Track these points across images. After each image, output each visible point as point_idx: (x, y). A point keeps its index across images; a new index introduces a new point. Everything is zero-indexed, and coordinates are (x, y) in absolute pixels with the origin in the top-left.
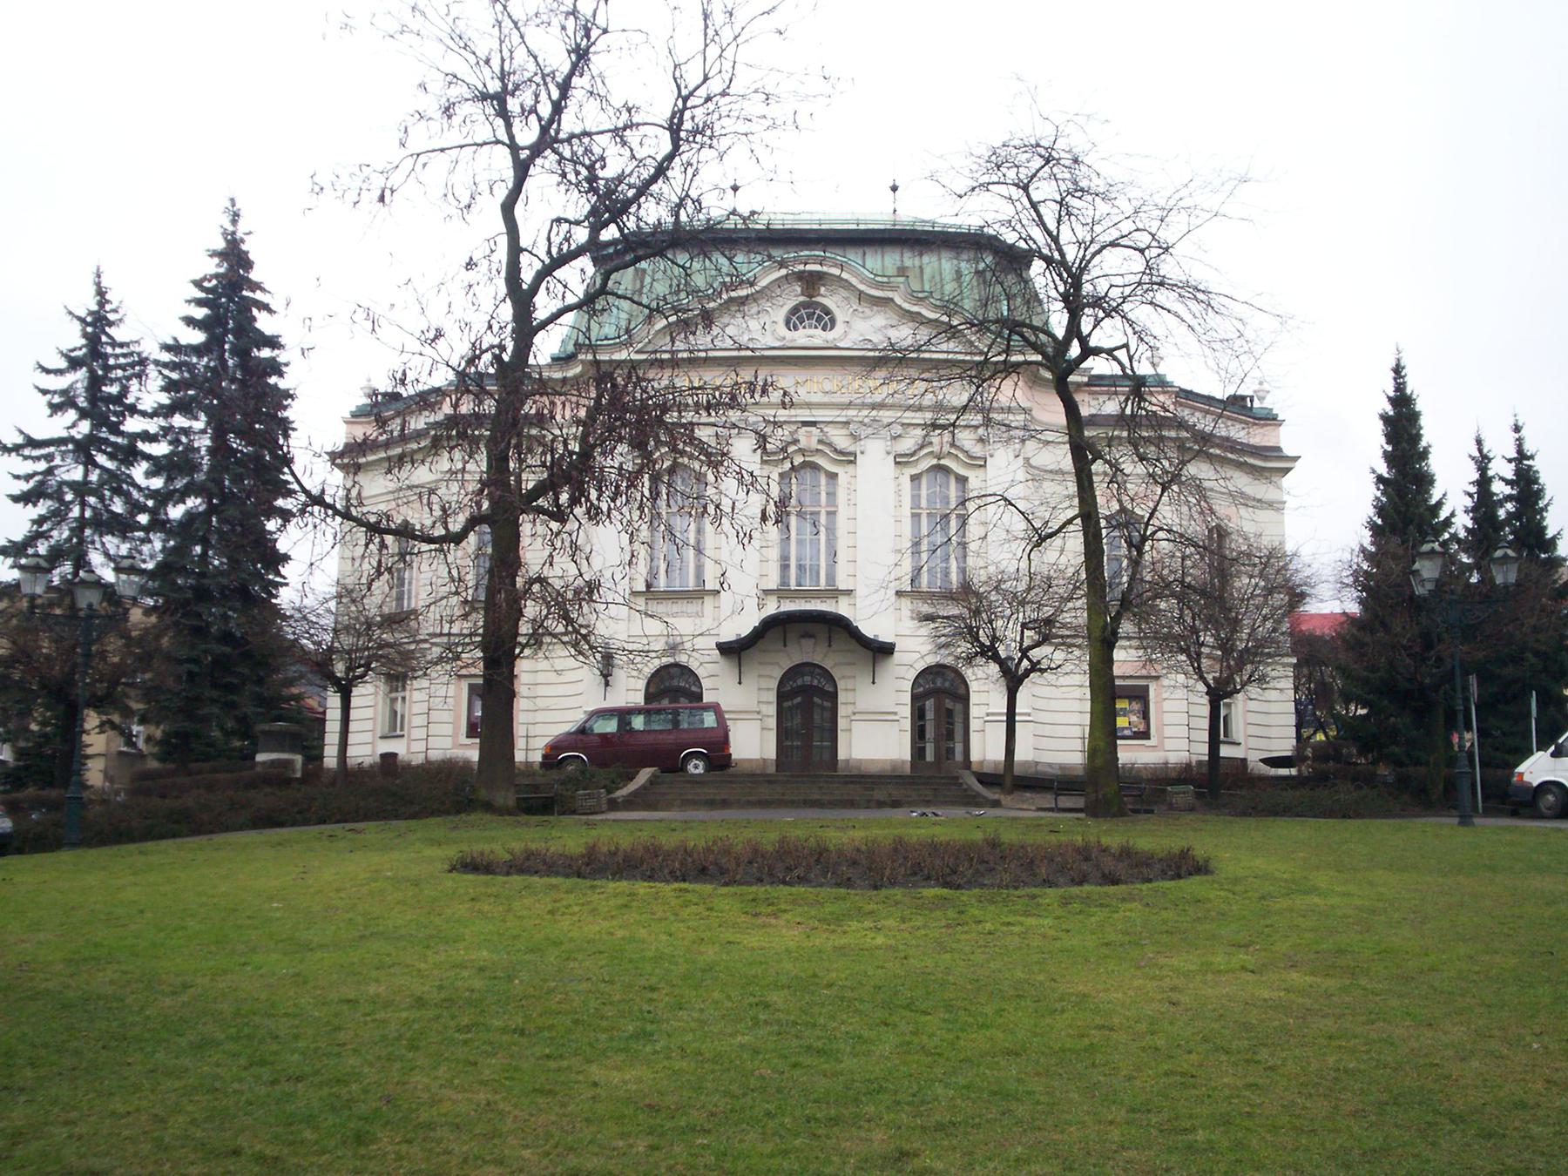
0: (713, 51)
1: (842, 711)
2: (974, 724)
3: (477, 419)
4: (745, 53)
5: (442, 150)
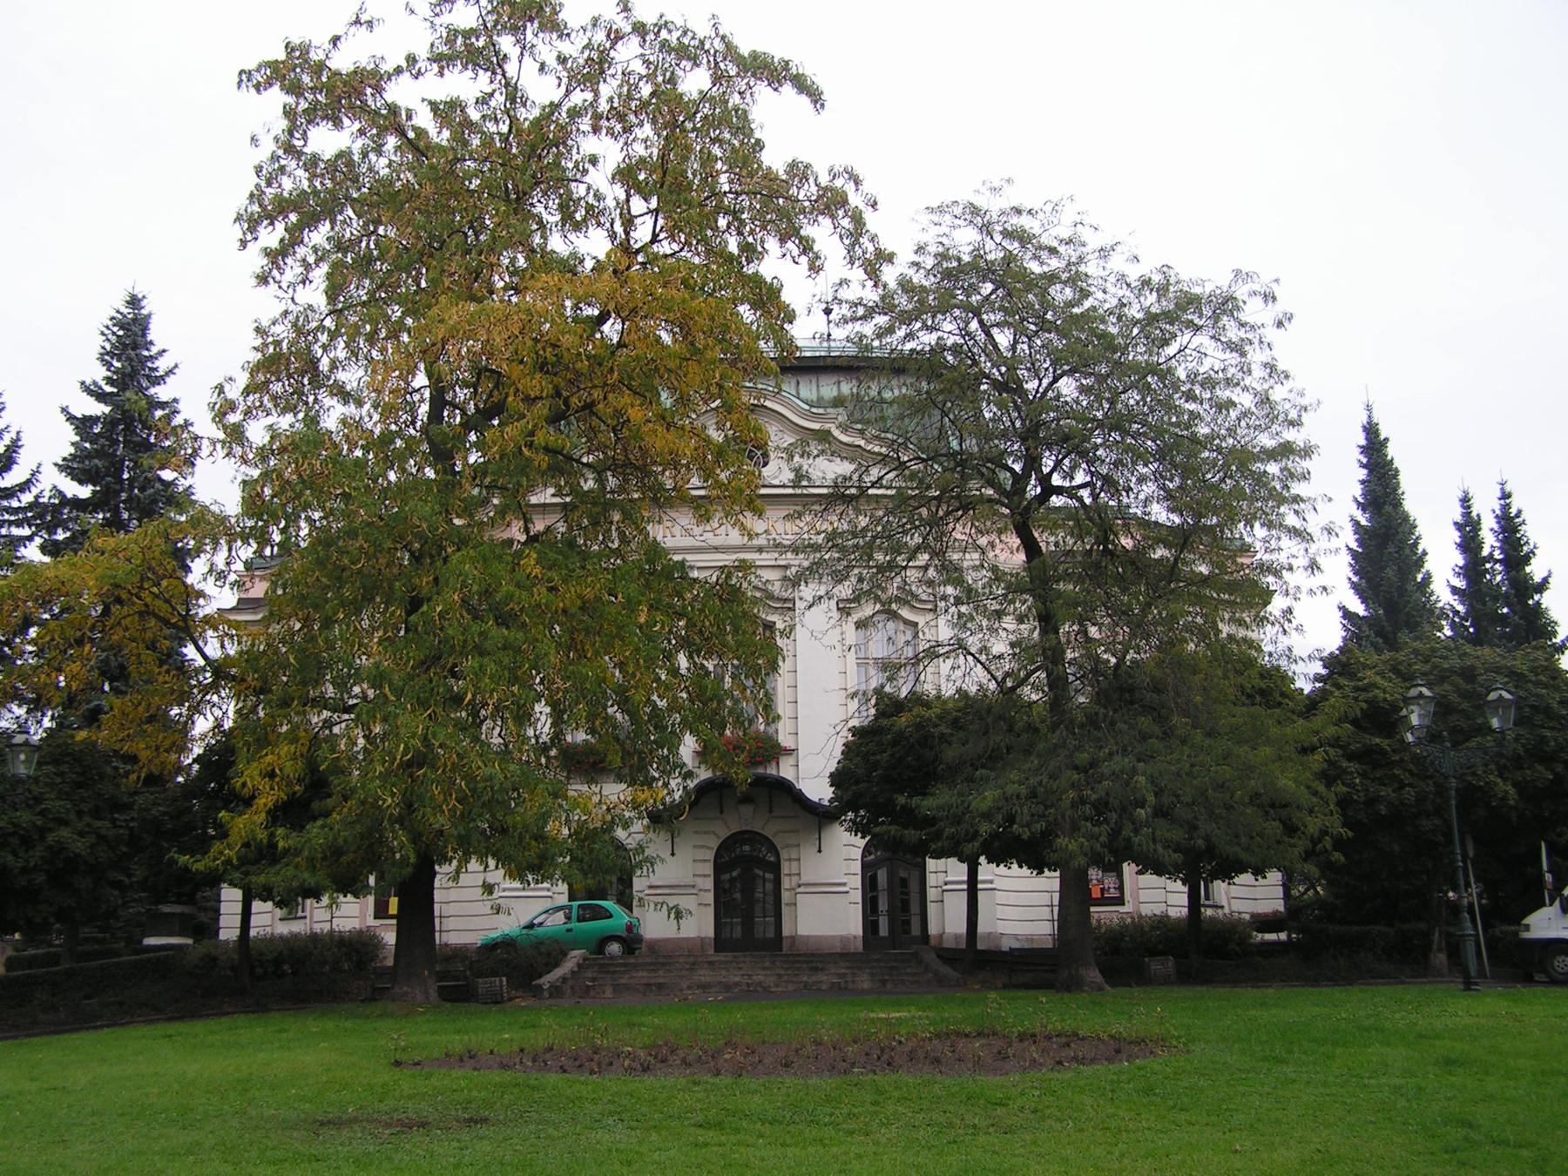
1: (786, 883)
2: (932, 894)
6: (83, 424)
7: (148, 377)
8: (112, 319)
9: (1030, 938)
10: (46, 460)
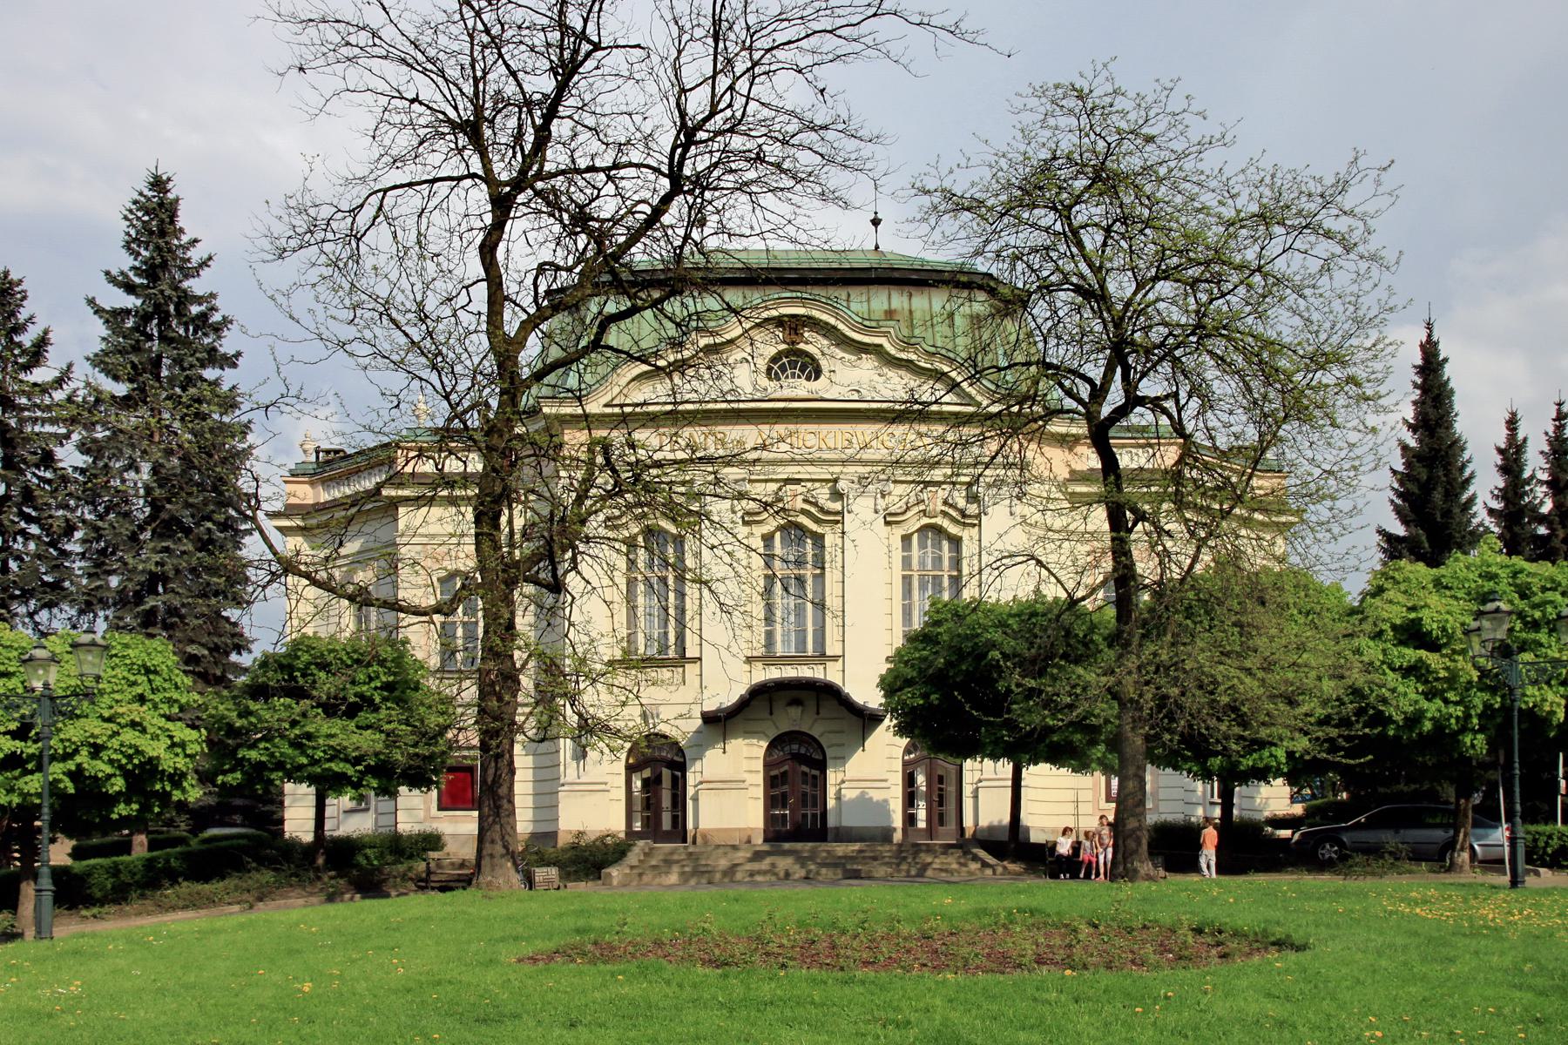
0: (723, 82)
3: (466, 479)
4: (761, 90)
5: (410, 185)
6: (114, 317)
7: (181, 268)
8: (135, 202)
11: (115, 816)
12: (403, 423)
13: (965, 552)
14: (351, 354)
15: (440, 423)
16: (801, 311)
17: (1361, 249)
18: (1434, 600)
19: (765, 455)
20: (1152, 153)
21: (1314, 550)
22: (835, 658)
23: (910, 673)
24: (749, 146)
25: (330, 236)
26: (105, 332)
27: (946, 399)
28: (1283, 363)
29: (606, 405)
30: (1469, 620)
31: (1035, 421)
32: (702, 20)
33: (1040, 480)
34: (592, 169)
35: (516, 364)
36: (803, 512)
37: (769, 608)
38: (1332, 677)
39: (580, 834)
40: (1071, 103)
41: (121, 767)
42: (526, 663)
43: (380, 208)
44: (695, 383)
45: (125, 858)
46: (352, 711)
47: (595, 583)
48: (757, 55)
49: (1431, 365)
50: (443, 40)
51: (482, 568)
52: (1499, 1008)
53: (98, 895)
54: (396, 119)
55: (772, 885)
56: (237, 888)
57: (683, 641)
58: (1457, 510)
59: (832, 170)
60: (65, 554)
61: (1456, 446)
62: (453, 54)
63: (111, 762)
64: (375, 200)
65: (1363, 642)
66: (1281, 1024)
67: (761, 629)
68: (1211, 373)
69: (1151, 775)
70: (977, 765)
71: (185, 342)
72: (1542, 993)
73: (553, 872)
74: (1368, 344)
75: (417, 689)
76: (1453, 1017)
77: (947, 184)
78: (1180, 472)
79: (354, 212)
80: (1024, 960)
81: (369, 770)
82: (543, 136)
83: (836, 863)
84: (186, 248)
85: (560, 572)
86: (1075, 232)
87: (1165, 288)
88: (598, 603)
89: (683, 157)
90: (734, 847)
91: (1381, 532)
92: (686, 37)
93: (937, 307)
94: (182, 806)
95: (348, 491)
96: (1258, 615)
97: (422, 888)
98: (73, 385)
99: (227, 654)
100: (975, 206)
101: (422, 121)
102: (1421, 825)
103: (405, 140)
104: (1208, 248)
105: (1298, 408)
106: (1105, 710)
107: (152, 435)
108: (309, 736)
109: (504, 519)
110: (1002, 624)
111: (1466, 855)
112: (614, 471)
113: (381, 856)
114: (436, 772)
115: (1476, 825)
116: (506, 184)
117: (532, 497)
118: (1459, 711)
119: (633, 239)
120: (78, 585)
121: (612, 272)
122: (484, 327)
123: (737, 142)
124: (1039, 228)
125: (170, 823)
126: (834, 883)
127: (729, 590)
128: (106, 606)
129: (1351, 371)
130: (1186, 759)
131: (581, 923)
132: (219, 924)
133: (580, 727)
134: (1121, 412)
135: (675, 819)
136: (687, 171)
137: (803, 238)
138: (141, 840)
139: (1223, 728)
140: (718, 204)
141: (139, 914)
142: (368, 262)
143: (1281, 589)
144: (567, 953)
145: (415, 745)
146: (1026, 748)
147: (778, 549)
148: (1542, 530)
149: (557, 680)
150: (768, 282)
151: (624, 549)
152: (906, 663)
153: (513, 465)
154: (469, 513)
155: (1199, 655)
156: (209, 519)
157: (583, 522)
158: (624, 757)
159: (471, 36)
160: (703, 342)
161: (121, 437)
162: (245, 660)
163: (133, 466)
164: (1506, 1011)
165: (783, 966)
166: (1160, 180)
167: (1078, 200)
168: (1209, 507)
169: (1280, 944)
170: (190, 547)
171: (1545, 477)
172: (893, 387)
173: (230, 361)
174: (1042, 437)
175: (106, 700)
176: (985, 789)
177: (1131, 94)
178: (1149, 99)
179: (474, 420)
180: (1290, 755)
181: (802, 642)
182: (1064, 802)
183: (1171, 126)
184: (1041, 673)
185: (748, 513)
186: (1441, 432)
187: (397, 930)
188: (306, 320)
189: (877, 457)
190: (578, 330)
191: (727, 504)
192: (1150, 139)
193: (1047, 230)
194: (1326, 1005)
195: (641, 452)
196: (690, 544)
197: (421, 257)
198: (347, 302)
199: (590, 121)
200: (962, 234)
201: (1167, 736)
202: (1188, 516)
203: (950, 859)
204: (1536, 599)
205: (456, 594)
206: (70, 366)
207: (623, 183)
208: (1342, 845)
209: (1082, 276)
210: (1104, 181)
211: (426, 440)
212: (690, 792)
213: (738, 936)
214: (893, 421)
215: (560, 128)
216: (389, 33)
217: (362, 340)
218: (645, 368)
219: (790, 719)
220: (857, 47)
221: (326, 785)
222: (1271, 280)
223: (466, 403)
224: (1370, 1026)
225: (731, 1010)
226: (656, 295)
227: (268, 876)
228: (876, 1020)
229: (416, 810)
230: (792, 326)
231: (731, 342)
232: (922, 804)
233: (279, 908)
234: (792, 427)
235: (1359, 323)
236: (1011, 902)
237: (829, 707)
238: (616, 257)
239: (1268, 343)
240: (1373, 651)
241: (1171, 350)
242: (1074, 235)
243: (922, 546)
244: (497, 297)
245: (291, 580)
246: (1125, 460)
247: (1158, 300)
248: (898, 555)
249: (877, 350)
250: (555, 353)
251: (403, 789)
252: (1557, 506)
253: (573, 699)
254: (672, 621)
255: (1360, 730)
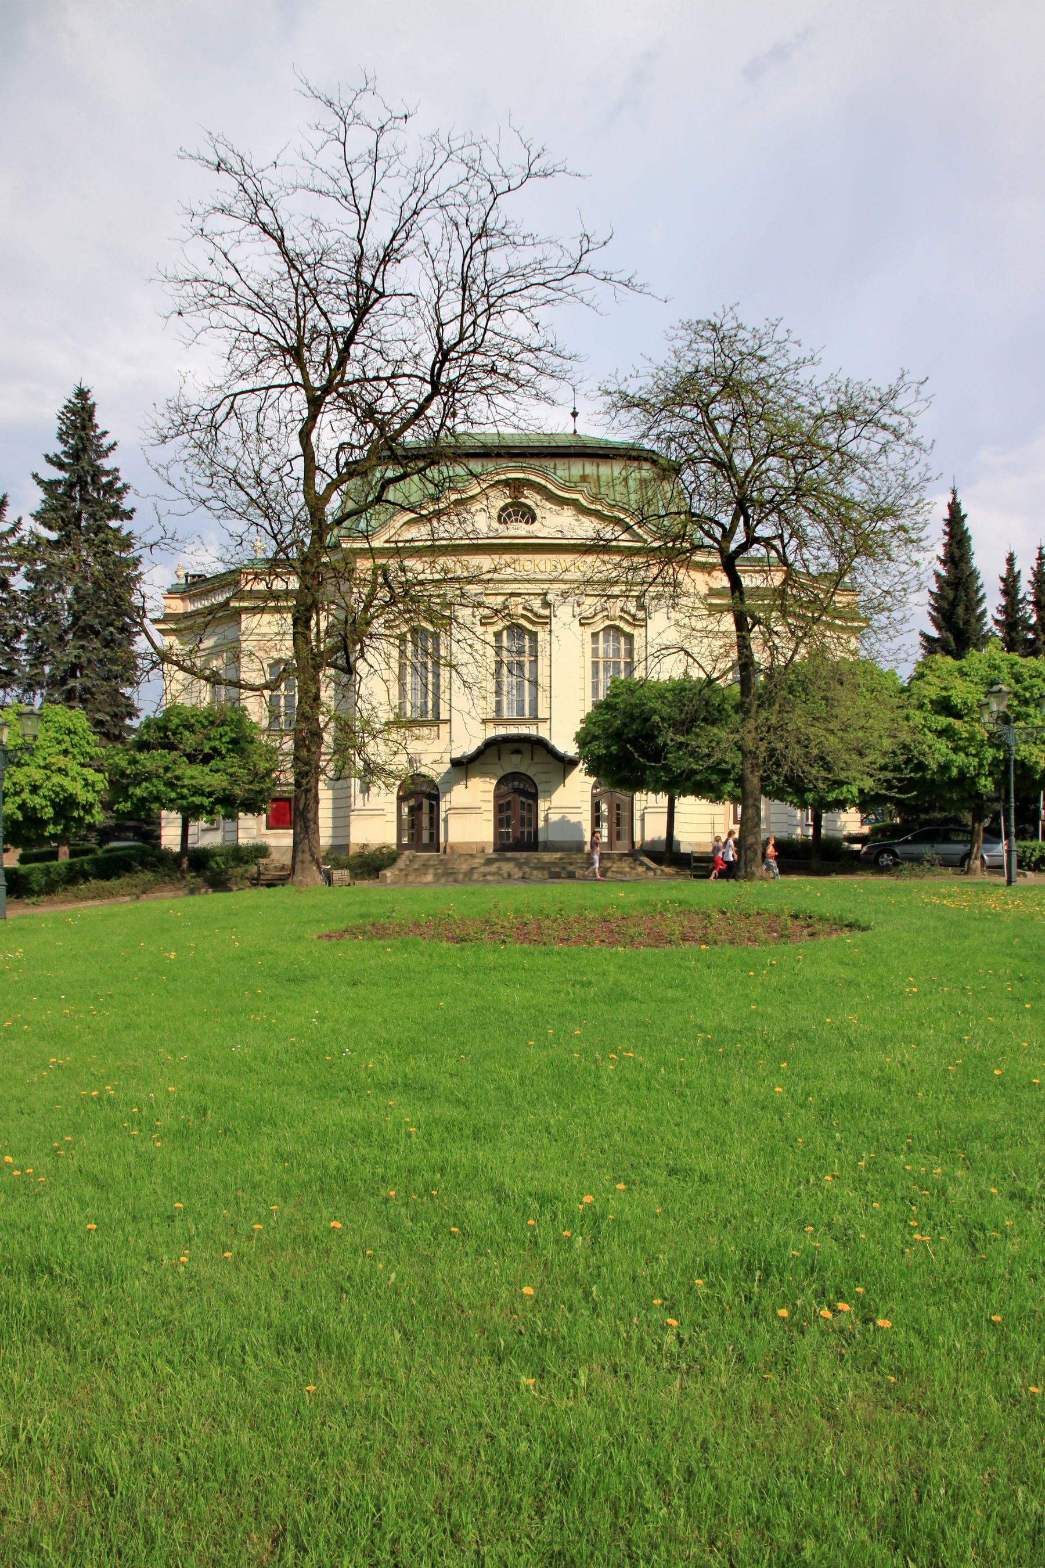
0: (469, 319)
3: (287, 594)
4: (495, 324)
5: (252, 391)
6: (49, 486)
7: (96, 452)
8: (66, 407)
9: (698, 844)
10: (27, 502)
11: (47, 834)
12: (244, 556)
13: (636, 645)
14: (210, 509)
15: (270, 555)
16: (521, 476)
17: (907, 437)
18: (958, 682)
19: (496, 576)
20: (764, 369)
21: (877, 647)
22: (544, 720)
23: (598, 732)
24: (486, 362)
25: (197, 427)
26: (44, 497)
27: (623, 537)
28: (855, 515)
29: (386, 542)
30: (982, 697)
31: (684, 553)
32: (454, 277)
33: (687, 594)
34: (377, 378)
35: (323, 513)
36: (523, 616)
37: (499, 685)
38: (889, 736)
39: (365, 846)
40: (708, 333)
41: (51, 800)
42: (327, 724)
43: (232, 407)
44: (447, 526)
45: (54, 863)
46: (207, 759)
47: (376, 667)
48: (492, 300)
49: (955, 520)
50: (277, 292)
51: (297, 656)
52: (996, 971)
53: (36, 888)
54: (244, 346)
55: (499, 882)
56: (128, 884)
57: (438, 707)
58: (973, 620)
59: (544, 379)
60: (15, 650)
61: (973, 575)
62: (284, 301)
63: (45, 797)
64: (228, 402)
65: (912, 712)
66: (850, 983)
67: (492, 699)
68: (805, 522)
69: (764, 804)
70: (644, 797)
71: (98, 502)
72: (1025, 960)
73: (346, 873)
74: (912, 503)
75: (252, 742)
76: (965, 977)
77: (623, 388)
78: (784, 590)
79: (214, 410)
80: (673, 938)
81: (218, 801)
82: (344, 357)
83: (543, 867)
84: (99, 438)
85: (352, 659)
86: (711, 423)
87: (773, 462)
88: (379, 681)
89: (440, 370)
90: (472, 855)
91: (922, 634)
92: (443, 288)
93: (616, 473)
94: (91, 827)
95: (207, 604)
96: (840, 693)
97: (254, 885)
98: (22, 533)
99: (123, 719)
100: (641, 404)
101: (261, 347)
102: (947, 840)
103: (248, 361)
104: (802, 434)
105: (866, 546)
106: (733, 758)
107: (74, 567)
108: (178, 778)
109: (313, 623)
110: (661, 697)
111: (978, 863)
112: (390, 587)
113: (225, 863)
114: (264, 801)
115: (985, 841)
116: (318, 389)
117: (333, 607)
118: (975, 761)
119: (405, 427)
120: (23, 672)
121: (390, 448)
122: (301, 488)
123: (478, 359)
124: (687, 419)
125: (84, 838)
126: (542, 881)
127: (469, 671)
128: (42, 687)
129: (901, 522)
130: (789, 794)
131: (364, 910)
132: (115, 909)
133: (365, 770)
134: (744, 548)
135: (431, 835)
136: (443, 379)
137: (523, 425)
138: (64, 851)
139: (814, 772)
140: (465, 402)
141: (63, 902)
142: (223, 444)
143: (854, 674)
144: (352, 932)
145: (251, 783)
146: (676, 785)
147: (505, 643)
148: (1030, 636)
149: (349, 736)
150: (499, 456)
151: (397, 642)
152: (594, 724)
153: (320, 584)
154: (289, 618)
155: (797, 720)
156: (111, 625)
157: (369, 624)
158: (395, 790)
159: (296, 289)
160: (453, 497)
161: (54, 569)
162: (135, 723)
163: (60, 589)
164: (1001, 972)
165: (504, 942)
166: (769, 388)
167: (713, 400)
168: (804, 615)
169: (850, 926)
170: (98, 645)
171: (1031, 598)
172: (585, 528)
173: (128, 515)
174: (691, 566)
175: (41, 753)
176: (649, 813)
177: (750, 328)
178: (762, 332)
179: (293, 553)
180: (861, 791)
181: (521, 709)
182: (702, 823)
183: (777, 351)
184: (688, 732)
185: (484, 617)
186: (963, 565)
187: (236, 915)
188: (179, 485)
189: (575, 578)
190: (366, 489)
191: (469, 611)
192: (762, 359)
193: (692, 420)
194: (881, 970)
195: (409, 574)
196: (444, 639)
197: (260, 440)
198: (208, 472)
199: (376, 345)
200: (633, 422)
201: (775, 778)
202: (790, 621)
203: (624, 864)
204: (1026, 684)
205: (281, 672)
206: (20, 519)
207: (398, 388)
208: (895, 855)
209: (715, 453)
210: (731, 388)
211: (261, 567)
212: (442, 815)
213: (474, 920)
214: (585, 553)
215: (356, 351)
216: (240, 288)
217: (217, 498)
218: (413, 515)
219: (513, 763)
220: (561, 295)
221: (190, 814)
222: (846, 458)
223: (288, 542)
224: (910, 984)
225: (466, 973)
226: (421, 464)
227: (149, 876)
228: (567, 981)
229: (251, 829)
230: (516, 486)
231: (472, 497)
232: (605, 825)
233: (156, 899)
234: (515, 557)
235: (906, 488)
236: (666, 896)
237: (541, 755)
238: (393, 439)
239: (844, 501)
240: (918, 717)
241: (778, 506)
242: (710, 424)
243: (606, 641)
244: (311, 468)
245: (167, 667)
246: (748, 581)
247: (768, 470)
248: (589, 646)
249: (574, 503)
250: (351, 505)
251: (241, 814)
252: (1040, 618)
253: (360, 749)
254: (430, 694)
255: (907, 774)
